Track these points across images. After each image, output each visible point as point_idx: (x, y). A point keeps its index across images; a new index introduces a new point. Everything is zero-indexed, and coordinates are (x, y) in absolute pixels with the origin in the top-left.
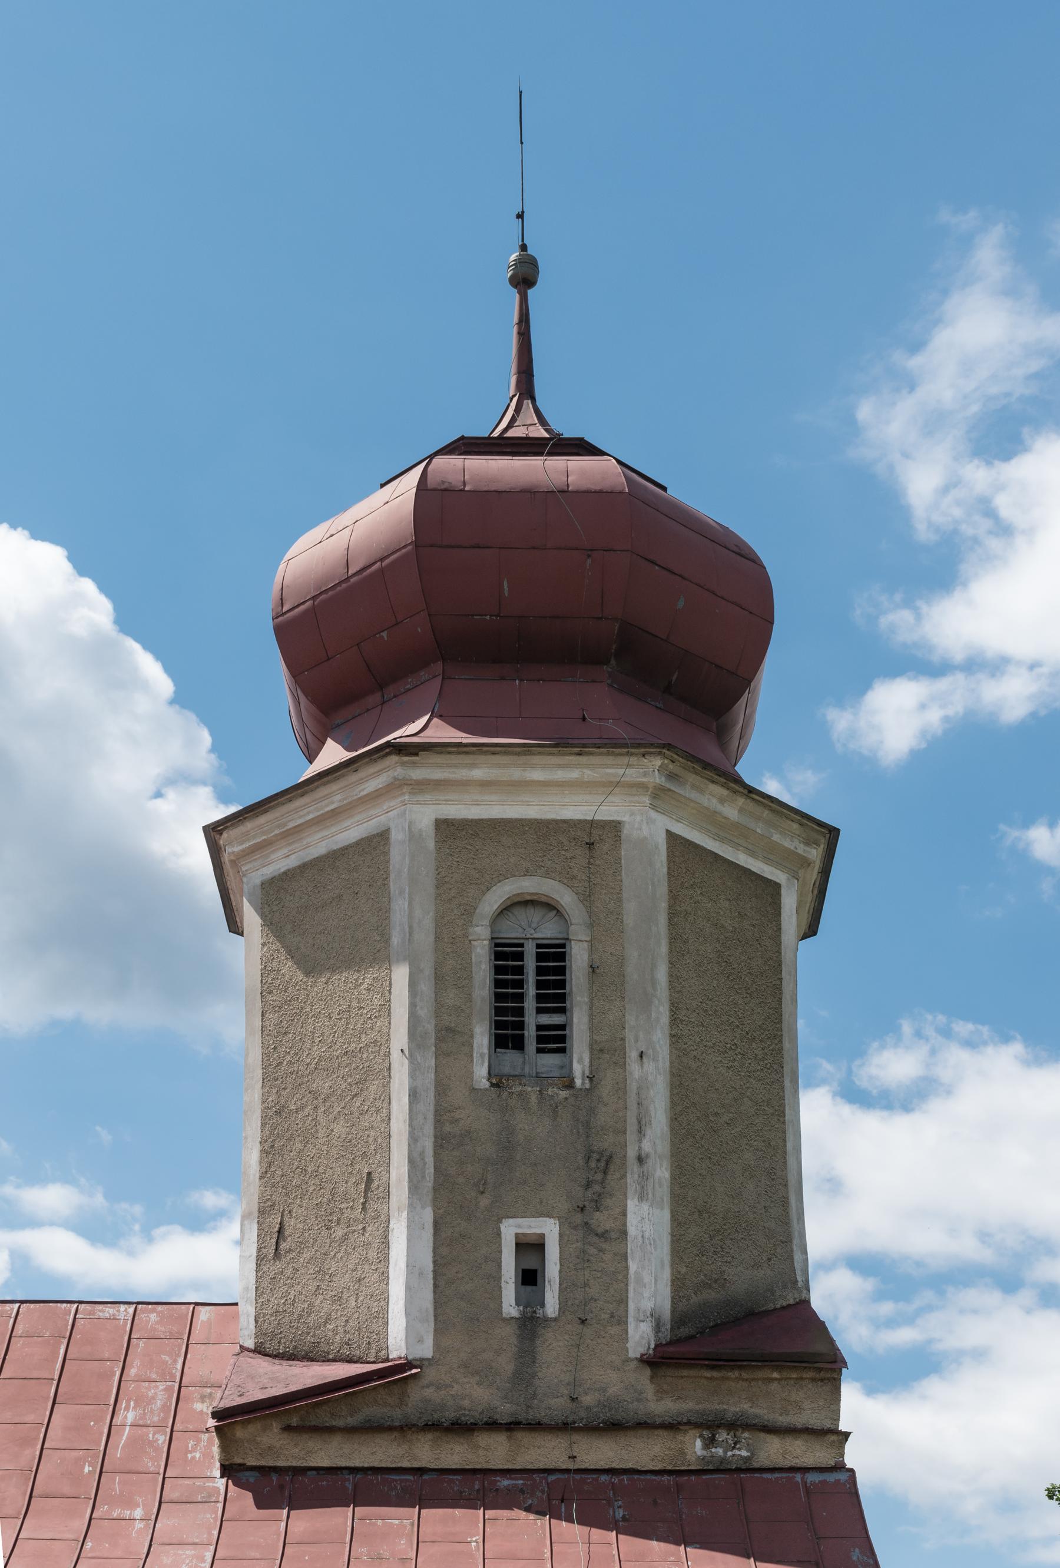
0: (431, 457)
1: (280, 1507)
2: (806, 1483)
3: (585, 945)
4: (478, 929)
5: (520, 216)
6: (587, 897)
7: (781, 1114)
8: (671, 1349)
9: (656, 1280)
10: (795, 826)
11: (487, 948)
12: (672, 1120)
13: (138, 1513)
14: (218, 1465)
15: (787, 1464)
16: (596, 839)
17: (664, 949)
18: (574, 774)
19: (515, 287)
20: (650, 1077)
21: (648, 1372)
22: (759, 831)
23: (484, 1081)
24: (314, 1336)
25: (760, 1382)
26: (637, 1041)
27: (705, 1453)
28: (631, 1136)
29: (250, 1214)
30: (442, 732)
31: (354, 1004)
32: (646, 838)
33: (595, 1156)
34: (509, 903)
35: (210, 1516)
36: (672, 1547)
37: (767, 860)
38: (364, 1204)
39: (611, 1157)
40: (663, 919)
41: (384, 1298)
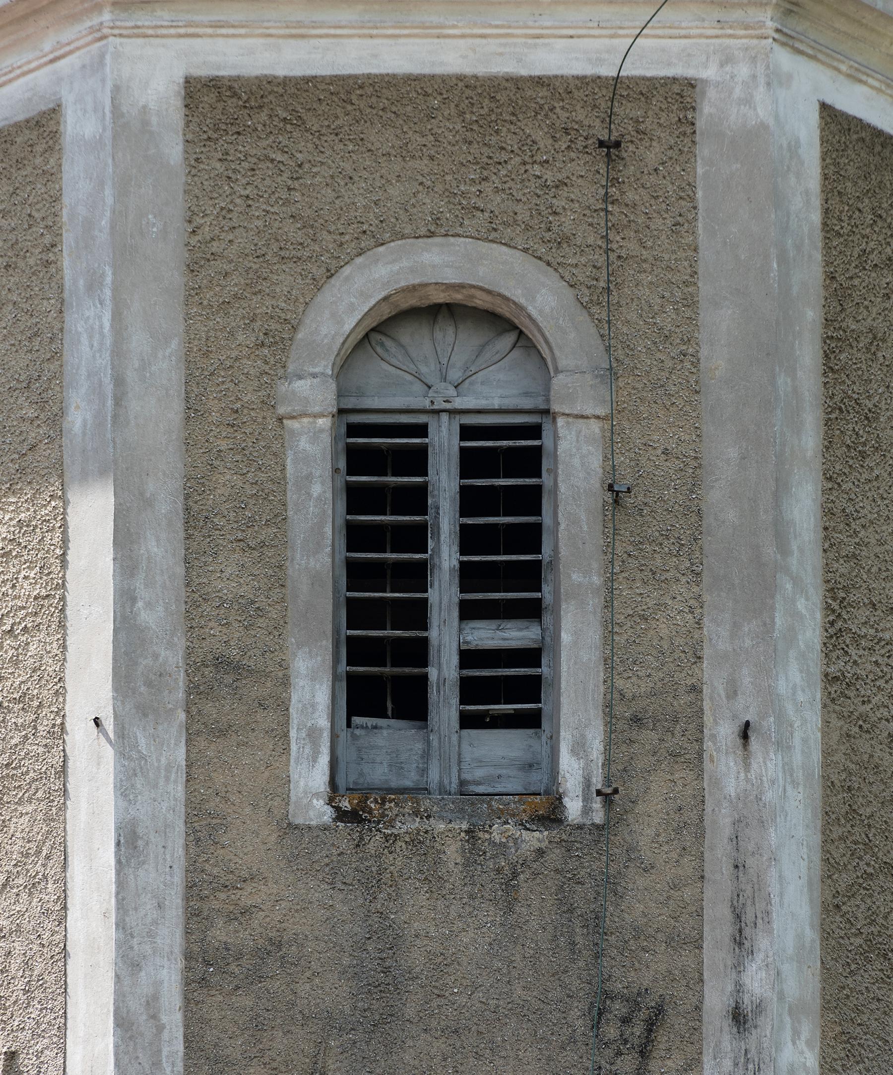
3: (595, 427)
6: (600, 296)
11: (326, 439)
17: (810, 440)
26: (733, 693)
28: (715, 952)
32: (764, 126)
33: (618, 1008)
34: (386, 312)
39: (659, 1010)
40: (808, 355)
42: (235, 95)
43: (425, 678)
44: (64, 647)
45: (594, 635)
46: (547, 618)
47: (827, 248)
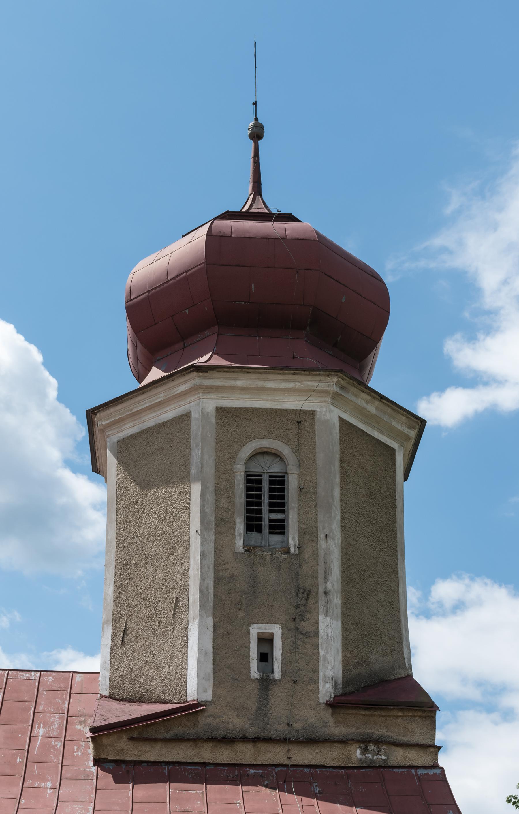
0: (214, 220)
1: (128, 783)
2: (418, 774)
3: (296, 476)
4: (238, 466)
5: (255, 104)
6: (297, 451)
7: (396, 572)
8: (343, 698)
9: (334, 660)
10: (404, 418)
11: (243, 477)
12: (342, 572)
13: (49, 785)
14: (92, 758)
15: (407, 764)
16: (302, 420)
17: (338, 480)
18: (291, 385)
19: (252, 139)
20: (331, 547)
21: (330, 711)
22: (385, 419)
23: (241, 548)
24: (144, 688)
25: (392, 718)
26: (324, 528)
27: (362, 757)
28: (321, 580)
29: (108, 621)
30: (218, 361)
31: (170, 506)
32: (328, 420)
33: (302, 591)
34: (255, 453)
35: (90, 786)
36: (348, 808)
37: (389, 436)
38: (174, 615)
39: (310, 591)
40: (337, 463)
41: (185, 667)
42: (226, 410)
43: (262, 524)
44: (190, 516)
45: (296, 516)
46: (286, 513)
47: (340, 443)
